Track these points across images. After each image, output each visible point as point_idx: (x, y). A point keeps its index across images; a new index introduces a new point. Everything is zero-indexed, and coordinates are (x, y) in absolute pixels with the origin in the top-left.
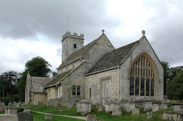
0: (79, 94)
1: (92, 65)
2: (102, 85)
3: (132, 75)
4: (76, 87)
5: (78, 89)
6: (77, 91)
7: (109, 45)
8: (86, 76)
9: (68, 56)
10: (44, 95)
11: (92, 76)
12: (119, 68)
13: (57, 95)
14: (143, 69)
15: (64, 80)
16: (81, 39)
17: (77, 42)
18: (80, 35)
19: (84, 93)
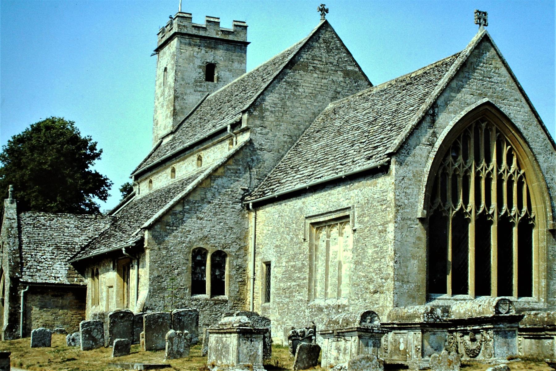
2: (313, 248)
3: (439, 200)
7: (349, 68)
13: (124, 295)
14: (483, 175)
17: (219, 55)
18: (231, 28)
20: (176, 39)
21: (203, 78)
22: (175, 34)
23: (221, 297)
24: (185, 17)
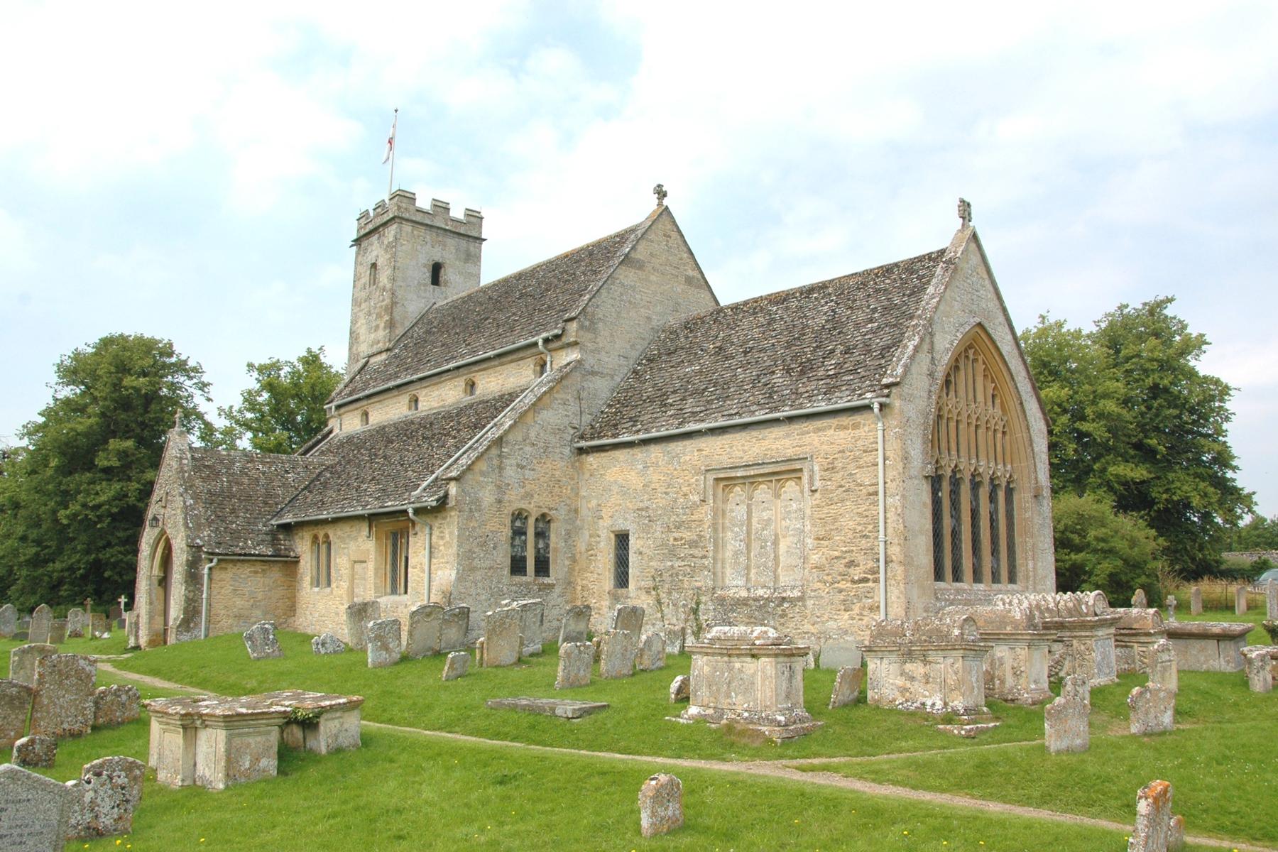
0: (542, 567)
1: (613, 384)
2: (719, 514)
4: (531, 521)
5: (541, 535)
6: (538, 550)
7: (690, 273)
8: (581, 451)
9: (400, 331)
10: (275, 574)
11: (639, 453)
12: (882, 406)
15: (469, 476)
16: (468, 234)
17: (447, 252)
19: (574, 560)
20: (395, 226)
21: (429, 281)
22: (393, 218)
23: (546, 580)
24: (406, 198)
